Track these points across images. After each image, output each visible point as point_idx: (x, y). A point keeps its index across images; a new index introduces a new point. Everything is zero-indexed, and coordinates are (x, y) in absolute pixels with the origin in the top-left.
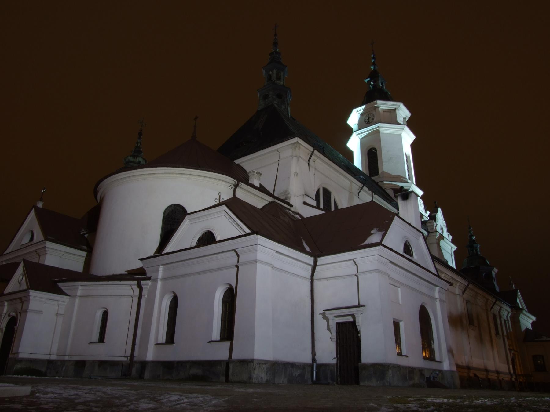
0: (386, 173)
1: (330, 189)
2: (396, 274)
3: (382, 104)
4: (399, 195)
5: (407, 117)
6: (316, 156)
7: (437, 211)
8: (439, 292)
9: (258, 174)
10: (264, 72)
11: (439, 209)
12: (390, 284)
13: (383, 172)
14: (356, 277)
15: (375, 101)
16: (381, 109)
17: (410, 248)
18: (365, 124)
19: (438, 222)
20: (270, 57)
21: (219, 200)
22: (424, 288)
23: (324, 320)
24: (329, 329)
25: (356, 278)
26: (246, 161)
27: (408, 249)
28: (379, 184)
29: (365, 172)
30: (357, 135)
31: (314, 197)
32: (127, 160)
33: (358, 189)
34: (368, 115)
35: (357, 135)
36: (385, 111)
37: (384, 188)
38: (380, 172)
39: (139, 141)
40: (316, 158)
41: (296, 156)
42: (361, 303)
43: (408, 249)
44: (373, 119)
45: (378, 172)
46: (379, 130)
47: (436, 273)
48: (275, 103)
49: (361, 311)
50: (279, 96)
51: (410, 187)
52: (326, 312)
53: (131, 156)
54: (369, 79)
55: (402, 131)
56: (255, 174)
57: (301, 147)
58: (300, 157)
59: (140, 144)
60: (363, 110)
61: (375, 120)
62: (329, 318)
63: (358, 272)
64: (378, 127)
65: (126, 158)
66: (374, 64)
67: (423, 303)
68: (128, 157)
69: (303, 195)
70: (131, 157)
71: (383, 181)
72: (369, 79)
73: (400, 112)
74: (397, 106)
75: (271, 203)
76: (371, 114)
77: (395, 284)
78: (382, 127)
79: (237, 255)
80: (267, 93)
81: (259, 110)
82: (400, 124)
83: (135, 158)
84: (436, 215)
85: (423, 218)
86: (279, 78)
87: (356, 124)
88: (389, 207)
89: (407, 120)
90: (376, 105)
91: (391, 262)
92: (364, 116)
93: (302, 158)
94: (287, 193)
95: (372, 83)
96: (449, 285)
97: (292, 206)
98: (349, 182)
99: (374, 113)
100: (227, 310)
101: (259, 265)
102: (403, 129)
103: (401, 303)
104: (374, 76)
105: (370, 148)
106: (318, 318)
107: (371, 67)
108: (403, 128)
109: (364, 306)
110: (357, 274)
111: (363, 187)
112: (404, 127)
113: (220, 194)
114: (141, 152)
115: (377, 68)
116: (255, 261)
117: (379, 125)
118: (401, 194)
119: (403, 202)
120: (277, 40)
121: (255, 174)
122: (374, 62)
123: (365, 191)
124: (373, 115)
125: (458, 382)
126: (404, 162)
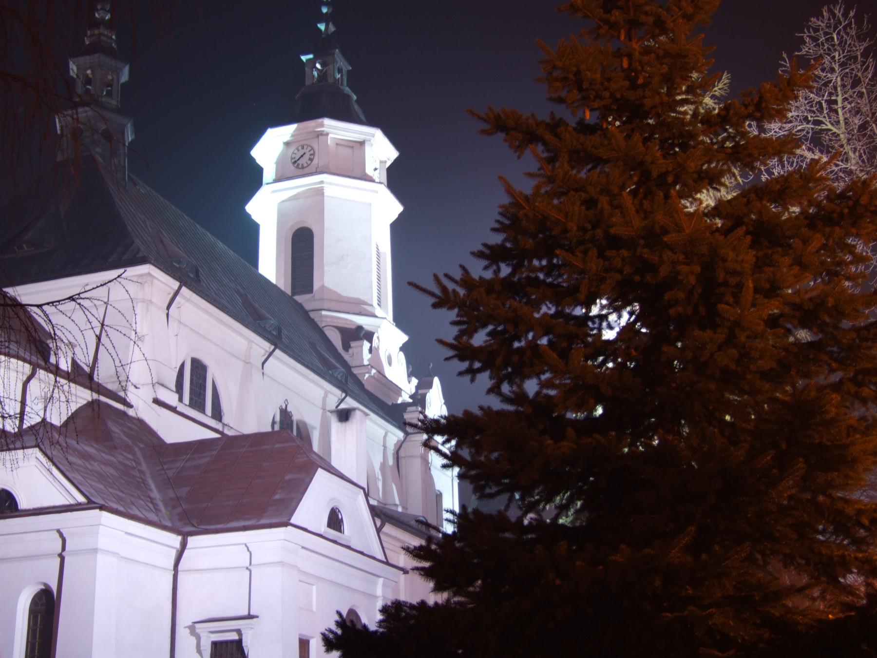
0: (329, 290)
1: (206, 360)
2: (312, 565)
5: (389, 159)
6: (185, 298)
7: (430, 386)
8: (384, 585)
11: (436, 381)
12: (300, 581)
13: (323, 287)
14: (247, 570)
16: (331, 138)
17: (340, 517)
19: (428, 409)
22: (357, 581)
23: (192, 636)
24: (199, 651)
25: (248, 572)
27: (335, 521)
28: (312, 315)
29: (282, 287)
31: (173, 385)
33: (263, 356)
34: (300, 148)
36: (340, 144)
37: (321, 325)
38: (316, 286)
40: (183, 301)
42: (252, 613)
43: (335, 521)
44: (311, 160)
45: (312, 290)
46: (323, 190)
47: (381, 556)
49: (252, 624)
51: (379, 327)
52: (197, 625)
62: (201, 635)
63: (252, 564)
64: (322, 182)
67: (354, 606)
71: (321, 310)
72: (311, 56)
74: (368, 136)
75: (92, 404)
76: (308, 146)
77: (308, 579)
78: (330, 184)
79: (61, 537)
84: (426, 393)
85: (401, 396)
89: (388, 165)
90: (322, 129)
91: (303, 548)
92: (292, 149)
95: (318, 66)
96: (402, 572)
97: (130, 406)
99: (316, 147)
100: (38, 625)
101: (101, 558)
103: (314, 609)
106: (182, 633)
109: (257, 617)
110: (249, 568)
111: (274, 351)
116: (95, 550)
119: (339, 424)
123: (277, 358)
124: (312, 149)
125: (21, 423)
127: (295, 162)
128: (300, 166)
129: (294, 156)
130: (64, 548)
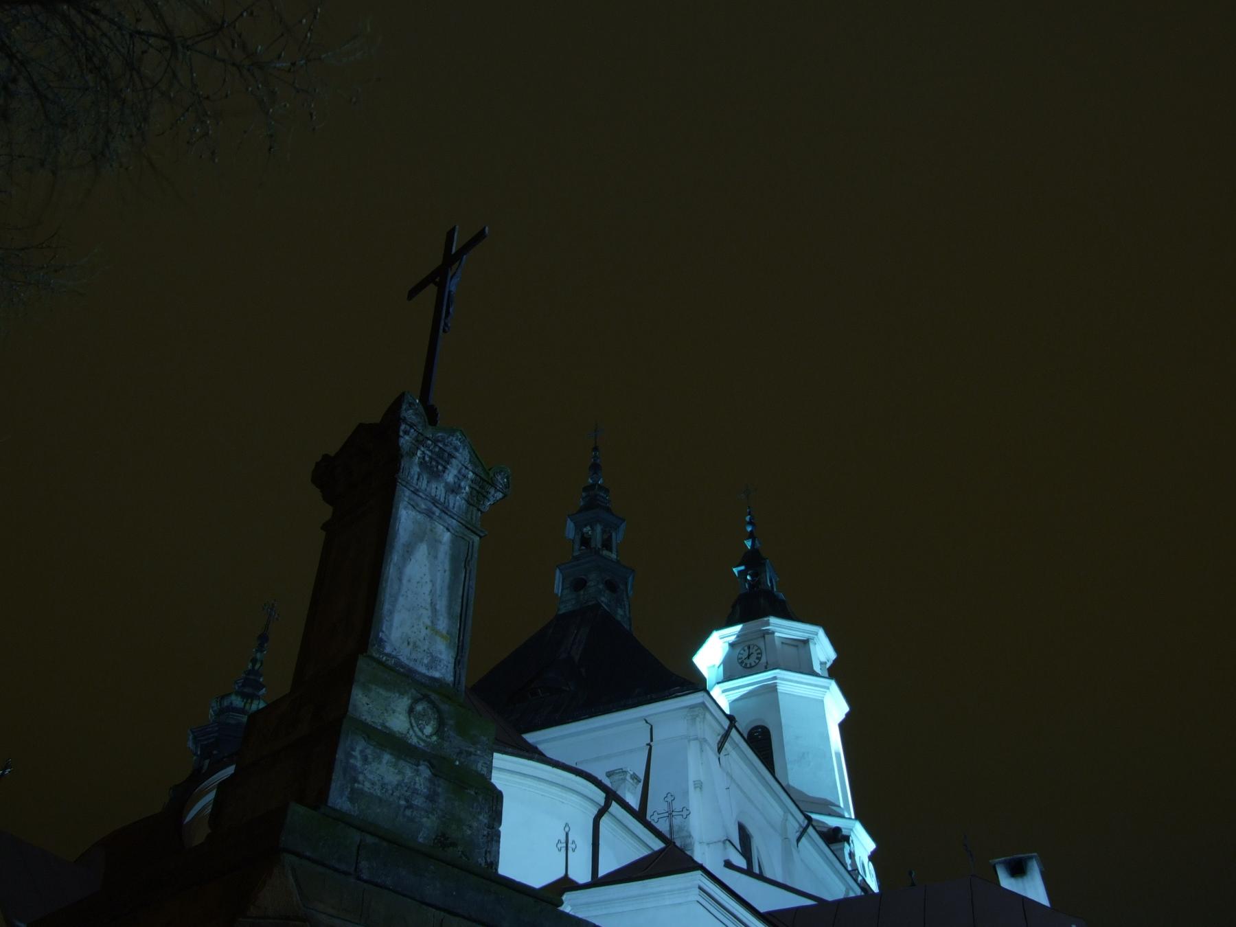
3: (780, 626)
4: (1000, 863)
9: (633, 780)
10: (570, 525)
15: (766, 619)
18: (740, 667)
20: (584, 494)
21: (564, 845)
26: (554, 739)
30: (724, 691)
32: (226, 703)
34: (746, 648)
35: (724, 691)
39: (259, 656)
41: (697, 739)
44: (759, 659)
46: (776, 686)
48: (602, 602)
50: (611, 586)
51: (852, 830)
53: (237, 693)
54: (742, 568)
55: (826, 692)
56: (628, 777)
57: (708, 716)
58: (705, 740)
59: (261, 665)
60: (735, 636)
61: (763, 660)
64: (775, 678)
65: (223, 697)
66: (751, 536)
68: (229, 695)
69: (724, 842)
70: (239, 699)
72: (742, 568)
73: (818, 647)
80: (583, 577)
81: (561, 612)
82: (817, 675)
83: (249, 701)
86: (607, 545)
87: (714, 666)
88: (848, 881)
89: (828, 665)
92: (737, 651)
93: (709, 745)
94: (684, 834)
98: (781, 812)
99: (762, 645)
102: (828, 688)
104: (753, 561)
105: (749, 728)
107: (745, 542)
108: (826, 685)
112: (831, 684)
113: (567, 829)
114: (261, 686)
115: (757, 544)
117: (775, 673)
118: (1005, 861)
120: (598, 461)
121: (628, 777)
122: (751, 531)
123: (810, 838)
124: (759, 648)
126: (833, 766)
127: (742, 662)
128: (748, 666)
129: (740, 656)
130: (652, 740)
